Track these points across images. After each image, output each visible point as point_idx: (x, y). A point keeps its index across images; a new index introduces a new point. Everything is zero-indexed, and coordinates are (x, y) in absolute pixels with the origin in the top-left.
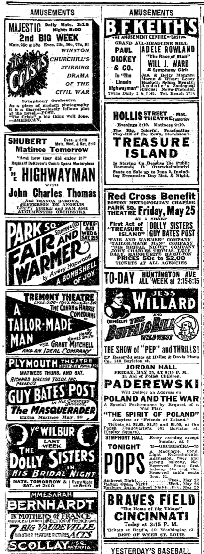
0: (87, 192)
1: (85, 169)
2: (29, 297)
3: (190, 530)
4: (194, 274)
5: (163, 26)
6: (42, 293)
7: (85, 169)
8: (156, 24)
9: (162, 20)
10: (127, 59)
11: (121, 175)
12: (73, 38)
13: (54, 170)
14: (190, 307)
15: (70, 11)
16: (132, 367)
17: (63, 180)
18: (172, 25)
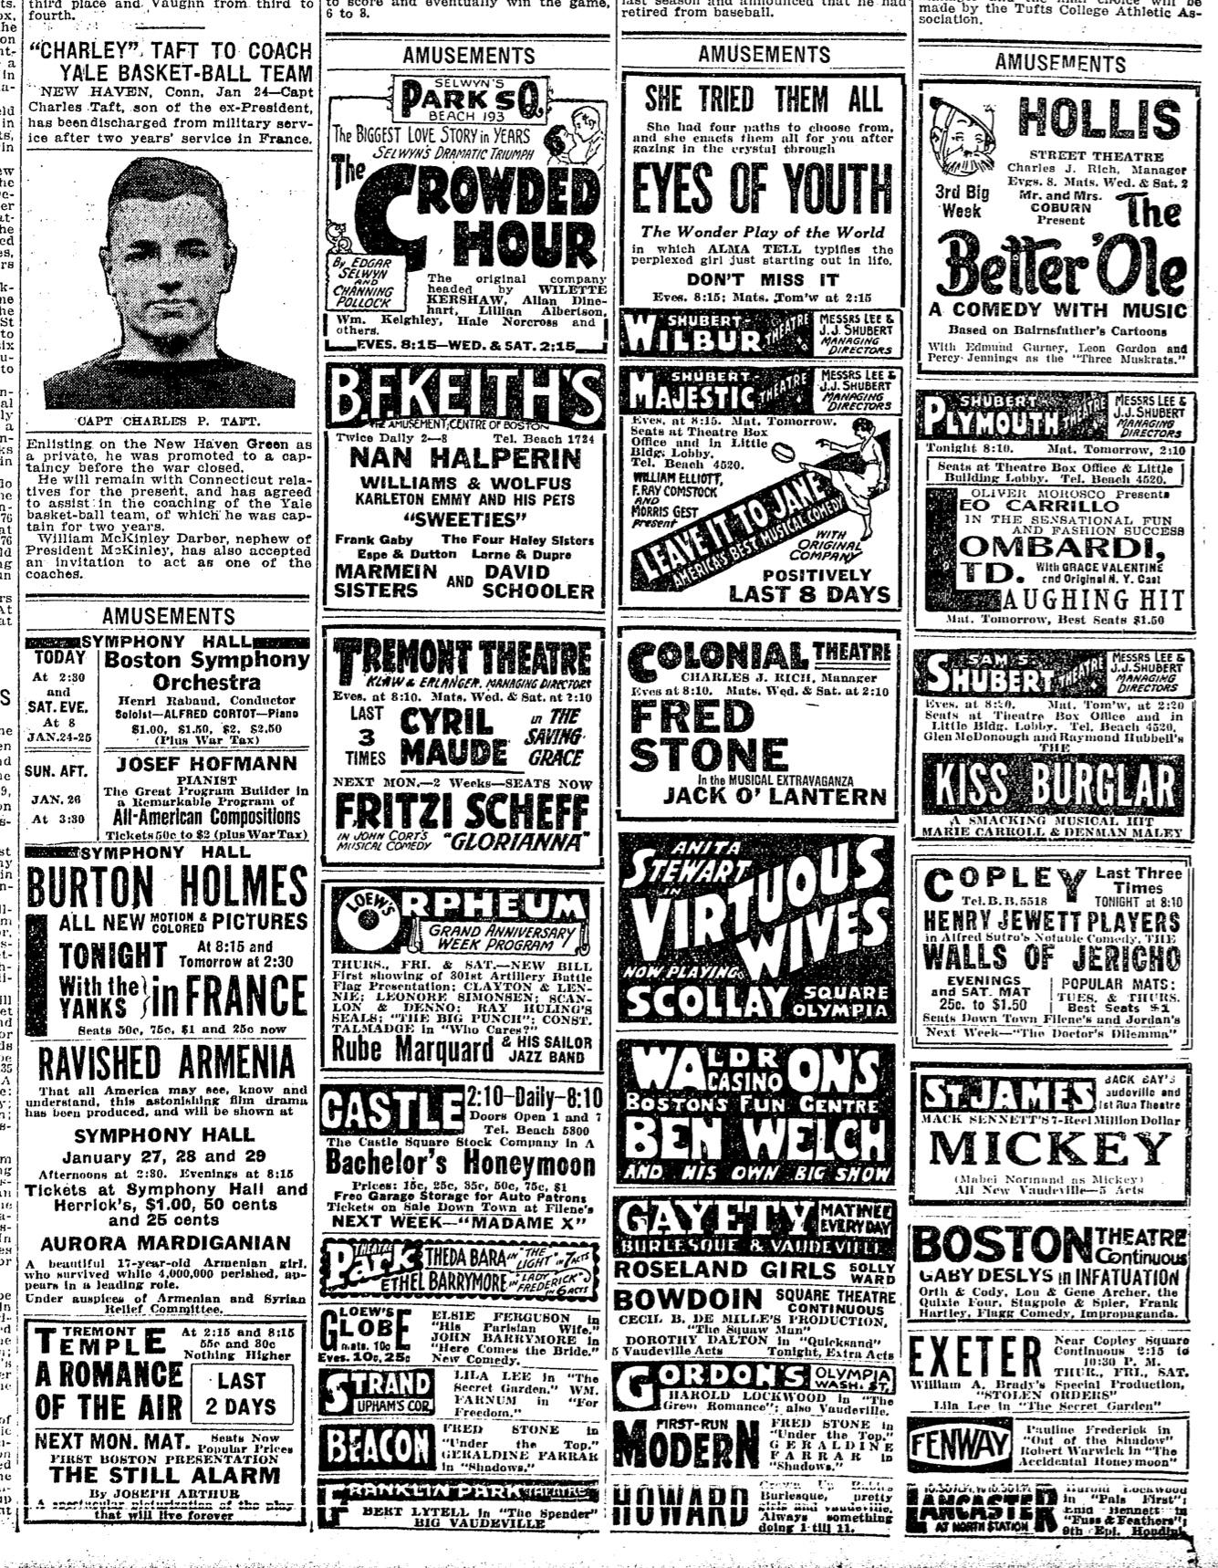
2: (358, 660)
4: (116, 1407)
5: (489, 388)
6: (407, 636)
8: (465, 383)
9: (484, 367)
10: (167, 72)
11: (211, 1109)
14: (420, 1391)
18: (515, 387)
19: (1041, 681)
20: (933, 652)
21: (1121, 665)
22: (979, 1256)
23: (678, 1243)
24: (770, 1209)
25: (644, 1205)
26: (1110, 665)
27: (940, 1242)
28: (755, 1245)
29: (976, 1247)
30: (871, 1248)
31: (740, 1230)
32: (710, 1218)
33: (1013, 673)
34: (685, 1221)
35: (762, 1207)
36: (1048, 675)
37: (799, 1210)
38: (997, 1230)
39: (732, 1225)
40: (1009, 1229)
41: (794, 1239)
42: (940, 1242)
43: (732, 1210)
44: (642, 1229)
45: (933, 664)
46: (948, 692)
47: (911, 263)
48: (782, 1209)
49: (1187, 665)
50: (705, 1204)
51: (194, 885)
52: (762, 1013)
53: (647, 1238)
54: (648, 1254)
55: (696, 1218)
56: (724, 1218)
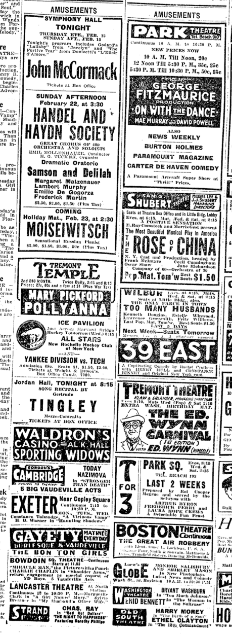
0: (42, 170)
1: (45, 110)
3: (215, 179)
7: (45, 110)
12: (45, 587)
13: (71, 235)
15: (195, 15)
16: (61, 211)
17: (38, 138)
19: (167, 204)
20: (129, 193)
21: (195, 199)
22: (140, 535)
23: (33, 545)
24: (65, 533)
25: (21, 532)
26: (192, 199)
27: (126, 530)
28: (60, 545)
29: (139, 532)
30: (101, 546)
31: (55, 540)
32: (44, 537)
33: (157, 201)
34: (36, 537)
35: (62, 532)
36: (169, 202)
37: (76, 533)
38: (146, 527)
39: (52, 539)
40: (150, 526)
41: (74, 543)
42: (126, 530)
43: (52, 533)
44: (21, 540)
45: (130, 197)
46: (135, 207)
47: (124, 55)
48: (70, 533)
49: (218, 200)
50: (43, 531)
51: (221, 615)
52: (76, 313)
53: (23, 543)
54: (23, 548)
55: (40, 536)
56: (49, 536)
